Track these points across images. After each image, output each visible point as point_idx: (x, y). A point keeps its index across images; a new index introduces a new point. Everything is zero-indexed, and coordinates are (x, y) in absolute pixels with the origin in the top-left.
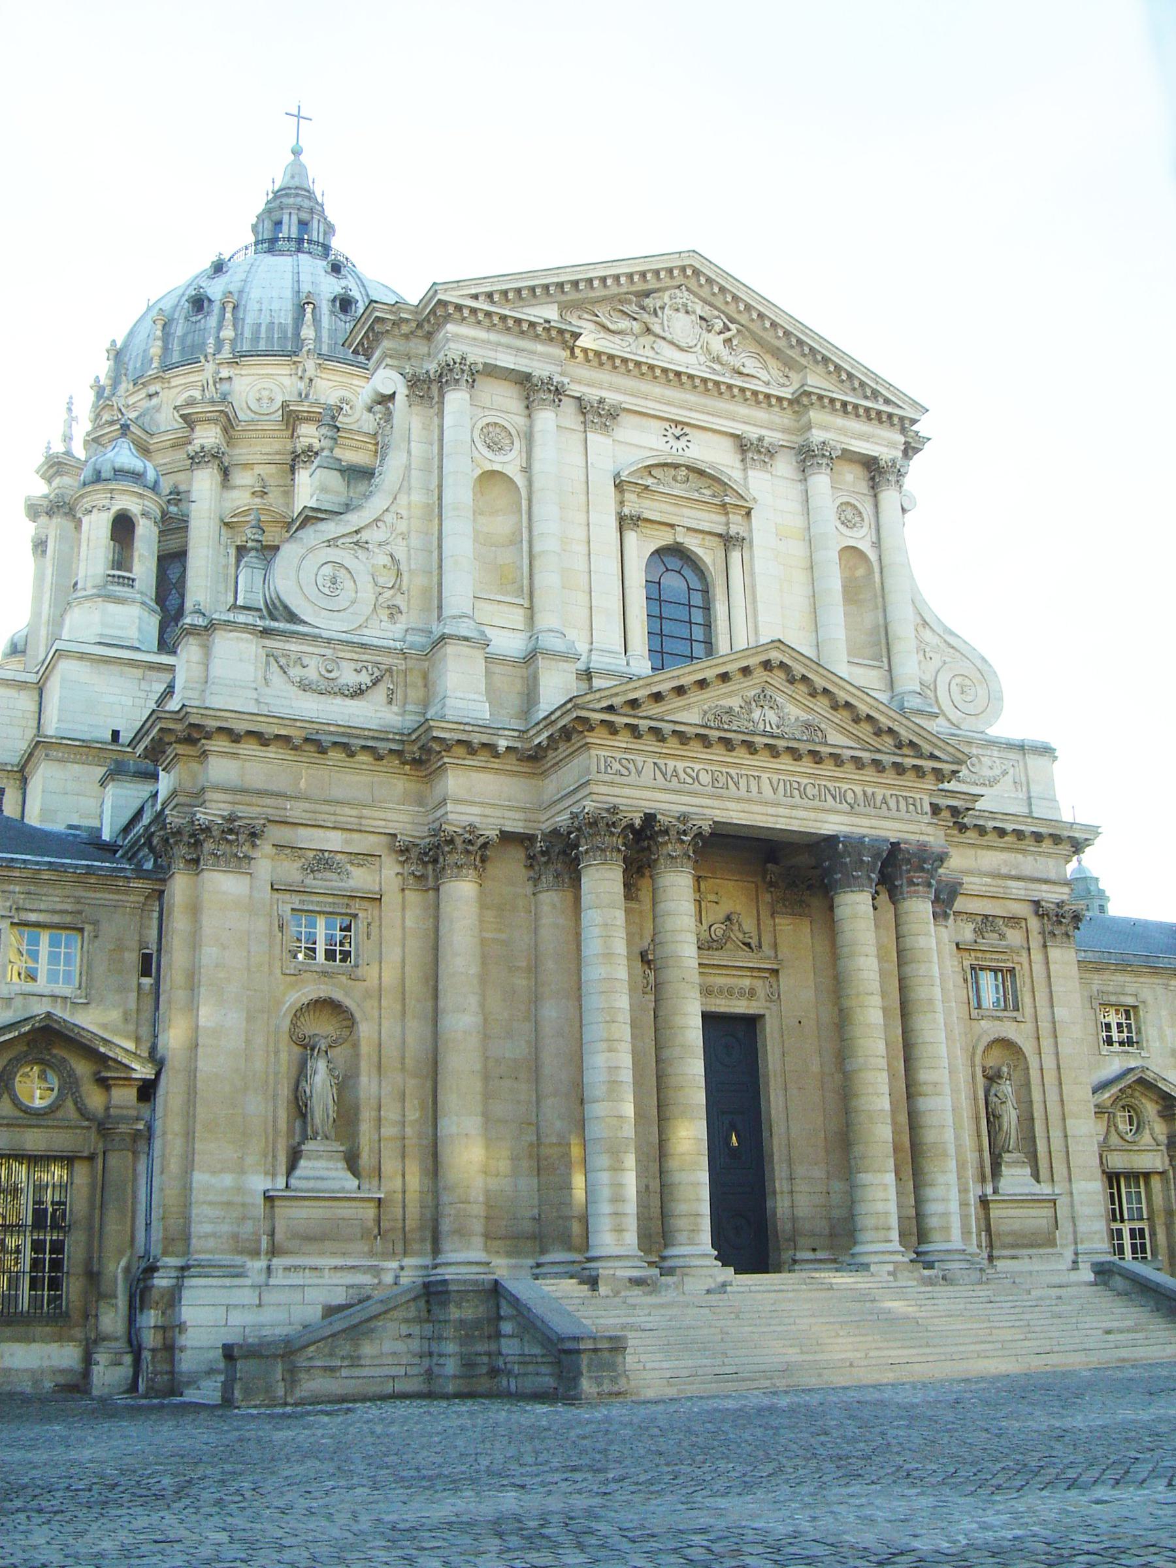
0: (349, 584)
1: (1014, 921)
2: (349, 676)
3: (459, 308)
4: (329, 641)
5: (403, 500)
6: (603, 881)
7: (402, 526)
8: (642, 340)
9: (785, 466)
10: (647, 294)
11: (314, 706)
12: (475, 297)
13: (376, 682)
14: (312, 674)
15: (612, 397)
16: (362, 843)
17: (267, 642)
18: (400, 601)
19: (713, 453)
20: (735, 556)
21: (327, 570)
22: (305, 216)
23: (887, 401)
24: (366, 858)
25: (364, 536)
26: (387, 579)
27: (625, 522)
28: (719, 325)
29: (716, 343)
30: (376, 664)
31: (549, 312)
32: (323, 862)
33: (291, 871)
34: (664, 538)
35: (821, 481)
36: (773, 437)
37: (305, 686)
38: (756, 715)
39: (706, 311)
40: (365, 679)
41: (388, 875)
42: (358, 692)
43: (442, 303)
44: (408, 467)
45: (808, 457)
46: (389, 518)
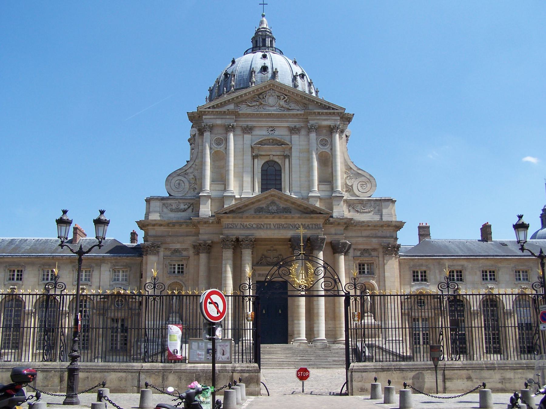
0: (183, 184)
1: (374, 250)
2: (182, 206)
3: (205, 112)
4: (177, 199)
5: (197, 161)
6: (228, 254)
7: (197, 167)
8: (260, 106)
9: (303, 132)
10: (261, 94)
11: (173, 215)
12: (209, 108)
13: (189, 208)
14: (174, 207)
15: (250, 124)
16: (184, 247)
17: (163, 202)
18: (196, 186)
19: (281, 133)
20: (287, 160)
21: (177, 182)
22: (264, 37)
23: (333, 109)
24: (186, 250)
25: (187, 171)
26: (193, 181)
27: (254, 157)
28: (282, 97)
29: (282, 103)
30: (189, 203)
31: (231, 107)
32: (176, 251)
33: (168, 253)
34: (266, 159)
35: (313, 135)
36: (298, 125)
37: (172, 210)
38: (270, 208)
39: (279, 94)
40: (186, 207)
41: (191, 252)
42: (185, 210)
43: (201, 112)
44: (198, 152)
45: (310, 130)
46: (194, 166)
